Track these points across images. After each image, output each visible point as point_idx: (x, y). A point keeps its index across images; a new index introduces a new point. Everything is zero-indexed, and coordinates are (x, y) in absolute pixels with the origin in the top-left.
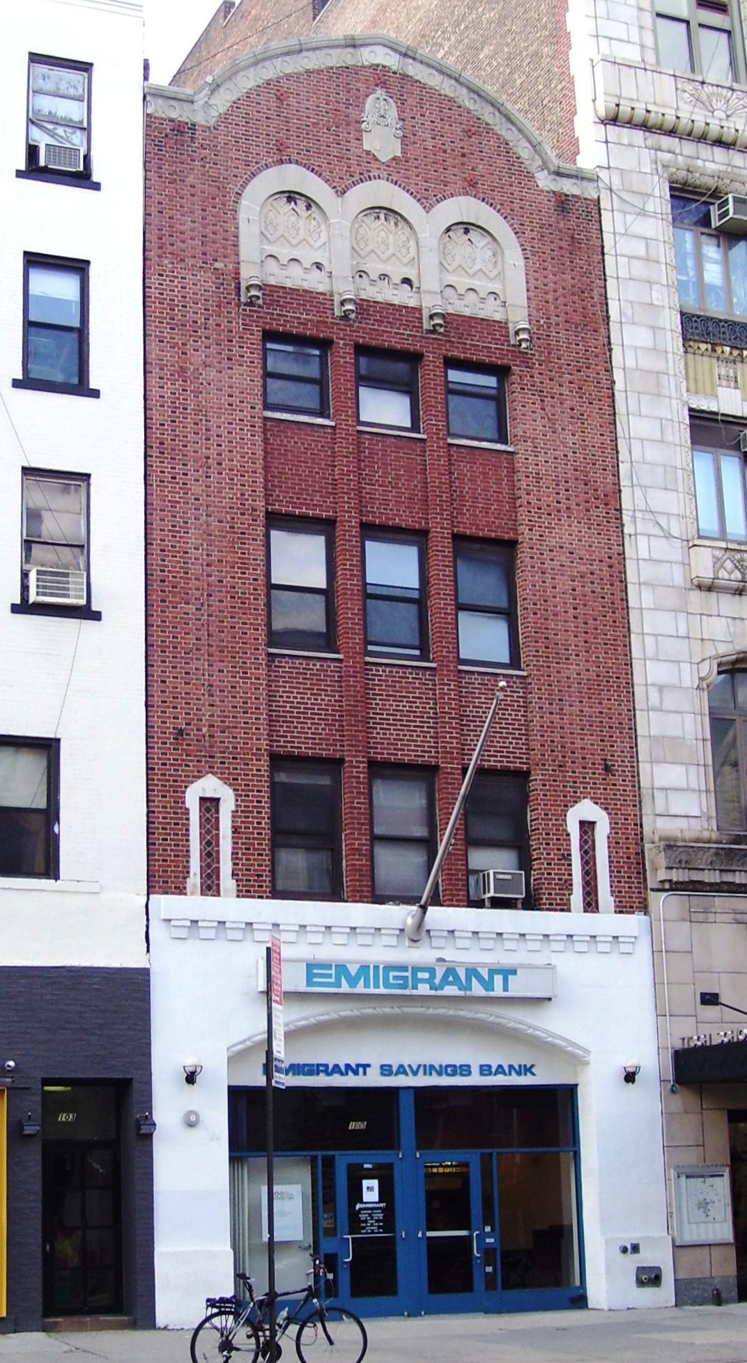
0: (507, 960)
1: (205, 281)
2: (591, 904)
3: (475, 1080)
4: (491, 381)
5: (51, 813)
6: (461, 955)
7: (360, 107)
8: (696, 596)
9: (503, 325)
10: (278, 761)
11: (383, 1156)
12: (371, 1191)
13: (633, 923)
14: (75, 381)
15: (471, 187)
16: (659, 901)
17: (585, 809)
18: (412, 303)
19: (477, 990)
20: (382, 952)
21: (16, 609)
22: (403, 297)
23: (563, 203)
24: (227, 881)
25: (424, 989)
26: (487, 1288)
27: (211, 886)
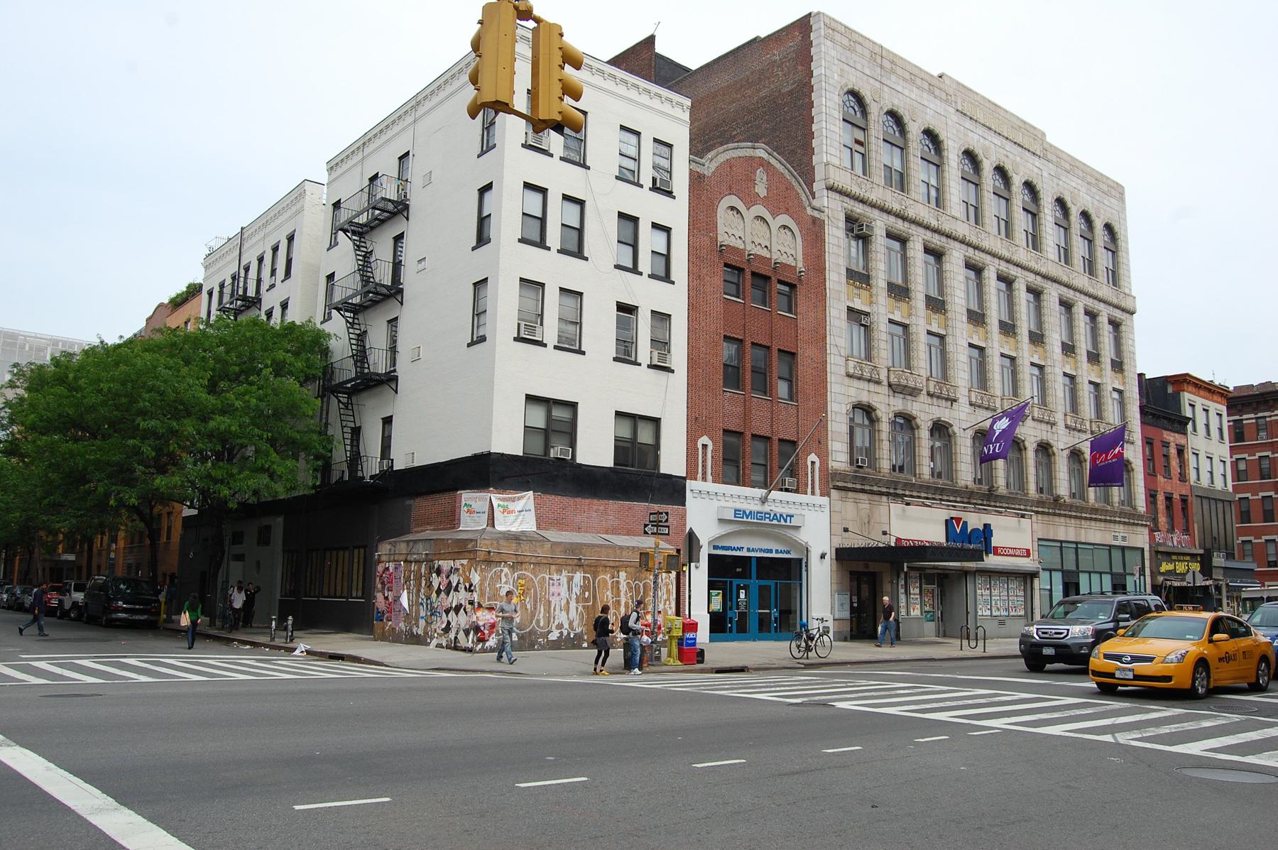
0: (791, 512)
1: (706, 241)
2: (813, 493)
3: (774, 555)
4: (787, 289)
5: (657, 446)
6: (779, 509)
7: (755, 173)
8: (847, 379)
9: (795, 268)
10: (726, 431)
11: (746, 582)
12: (742, 596)
13: (826, 499)
14: (663, 274)
15: (787, 211)
16: (834, 493)
17: (813, 457)
18: (742, 247)
19: (783, 522)
20: (755, 507)
21: (515, 339)
22: (765, 253)
23: (815, 221)
24: (709, 477)
25: (767, 521)
26: (761, 630)
27: (704, 479)
